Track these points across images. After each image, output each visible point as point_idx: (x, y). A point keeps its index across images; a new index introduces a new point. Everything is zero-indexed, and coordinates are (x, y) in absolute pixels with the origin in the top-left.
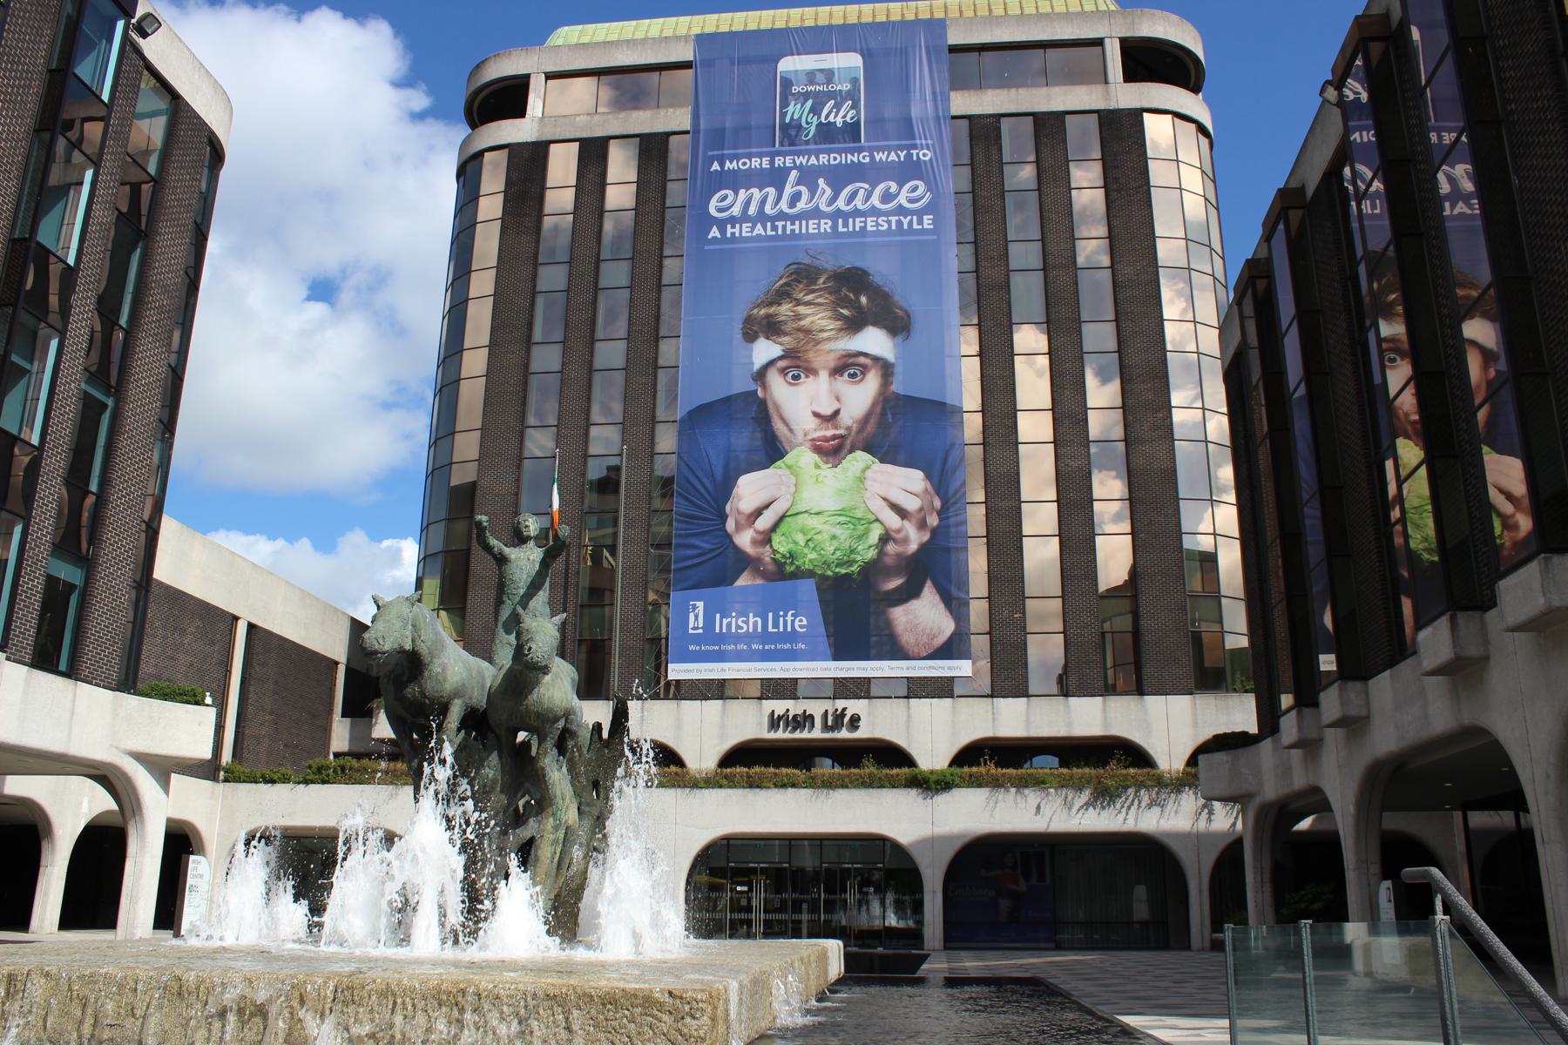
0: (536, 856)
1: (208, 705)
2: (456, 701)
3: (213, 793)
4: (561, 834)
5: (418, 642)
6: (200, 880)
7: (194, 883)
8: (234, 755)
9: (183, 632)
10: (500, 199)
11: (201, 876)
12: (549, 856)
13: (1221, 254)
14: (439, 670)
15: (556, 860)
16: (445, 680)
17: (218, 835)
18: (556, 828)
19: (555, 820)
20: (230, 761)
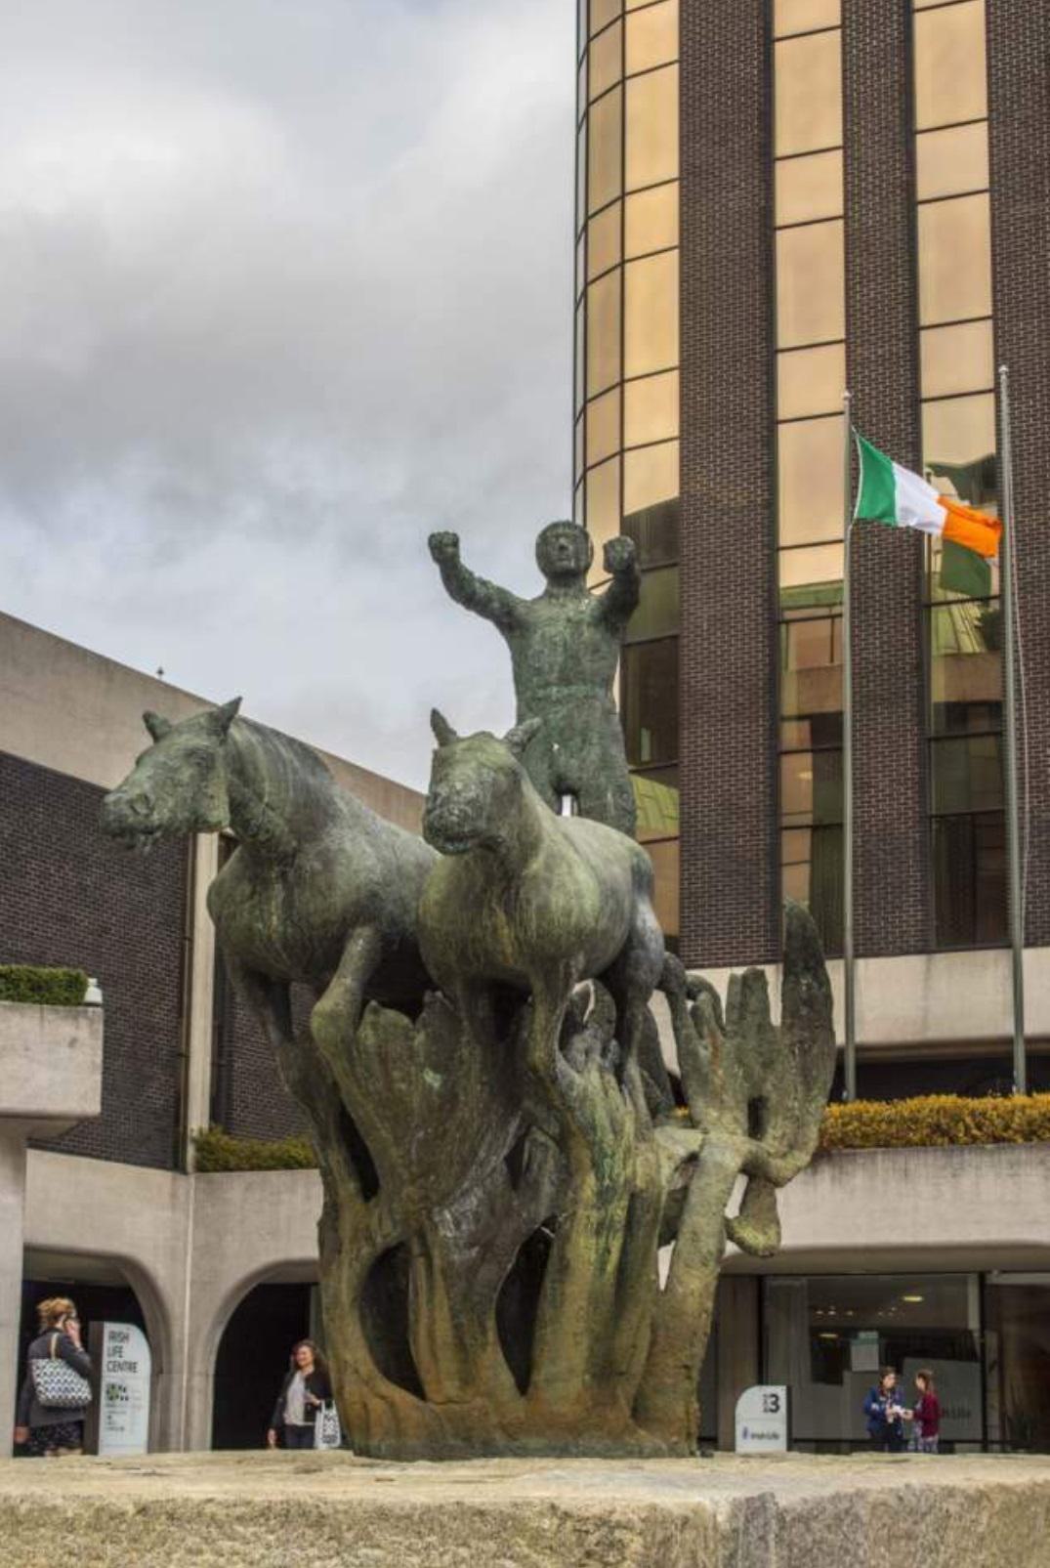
0: (562, 1258)
1: (974, 1272)
2: (359, 930)
3: (174, 1195)
4: (618, 1211)
5: (256, 810)
6: (127, 1374)
7: (113, 1381)
8: (214, 1116)
9: (998, 1116)
10: (833, 166)
11: (132, 1367)
12: (593, 1257)
13: (619, 23)
14: (317, 866)
15: (611, 1267)
16: (330, 887)
17: (193, 1283)
18: (604, 1196)
19: (600, 1178)
20: (206, 1126)
